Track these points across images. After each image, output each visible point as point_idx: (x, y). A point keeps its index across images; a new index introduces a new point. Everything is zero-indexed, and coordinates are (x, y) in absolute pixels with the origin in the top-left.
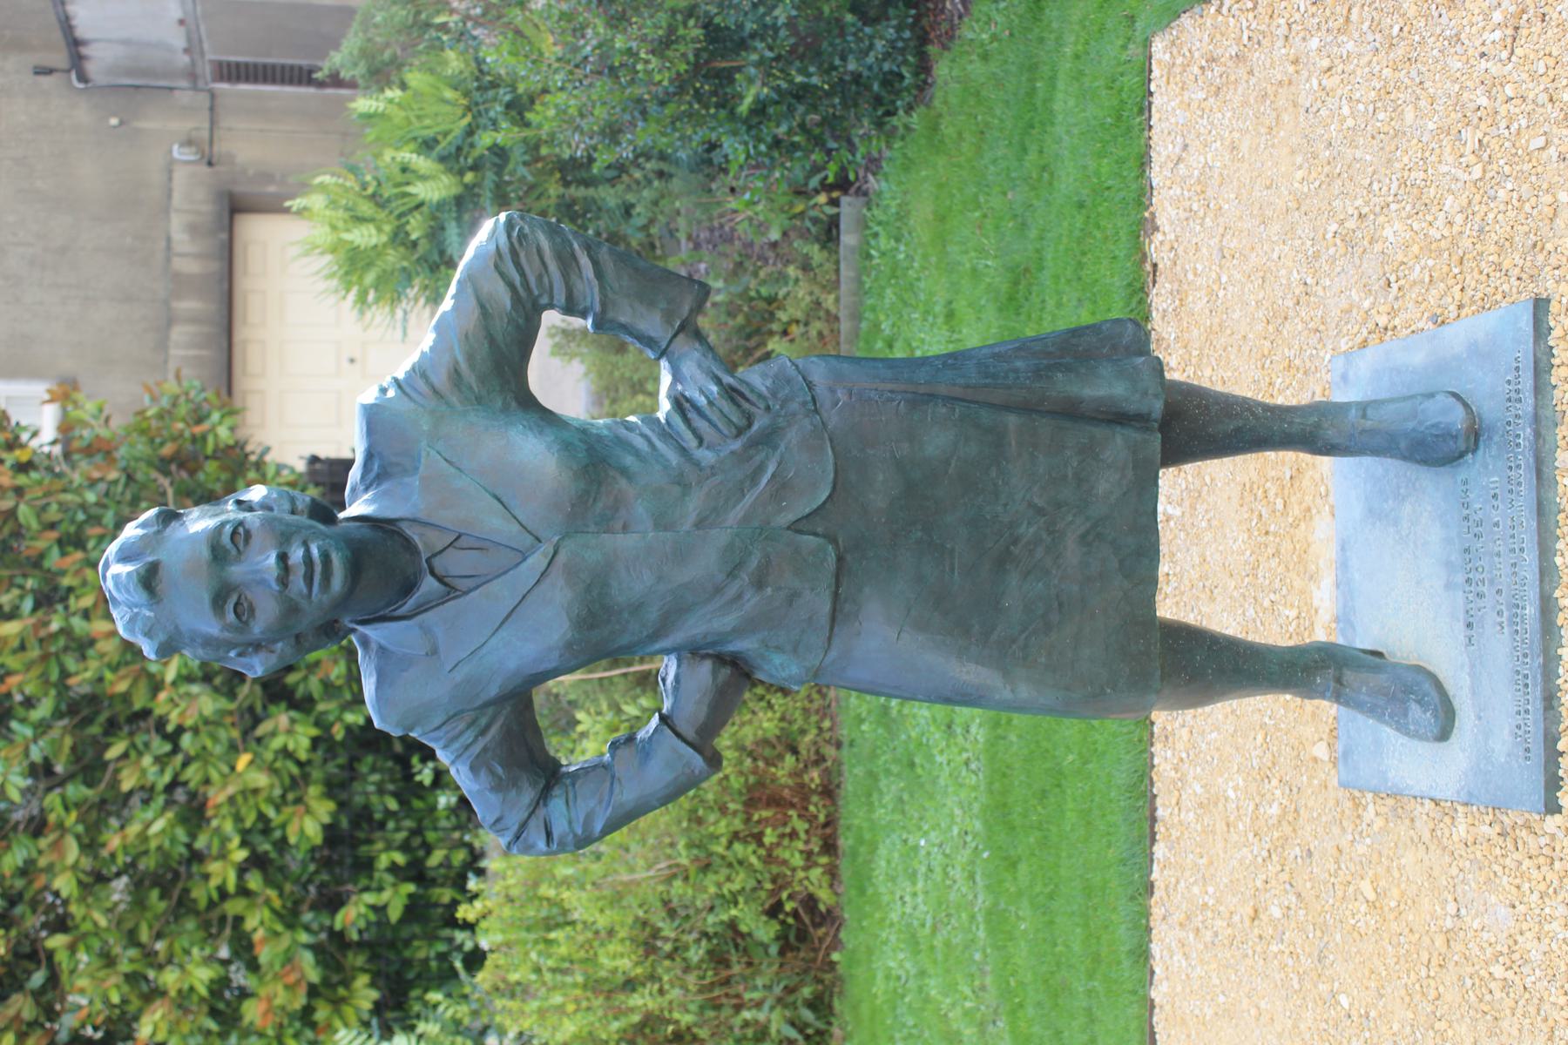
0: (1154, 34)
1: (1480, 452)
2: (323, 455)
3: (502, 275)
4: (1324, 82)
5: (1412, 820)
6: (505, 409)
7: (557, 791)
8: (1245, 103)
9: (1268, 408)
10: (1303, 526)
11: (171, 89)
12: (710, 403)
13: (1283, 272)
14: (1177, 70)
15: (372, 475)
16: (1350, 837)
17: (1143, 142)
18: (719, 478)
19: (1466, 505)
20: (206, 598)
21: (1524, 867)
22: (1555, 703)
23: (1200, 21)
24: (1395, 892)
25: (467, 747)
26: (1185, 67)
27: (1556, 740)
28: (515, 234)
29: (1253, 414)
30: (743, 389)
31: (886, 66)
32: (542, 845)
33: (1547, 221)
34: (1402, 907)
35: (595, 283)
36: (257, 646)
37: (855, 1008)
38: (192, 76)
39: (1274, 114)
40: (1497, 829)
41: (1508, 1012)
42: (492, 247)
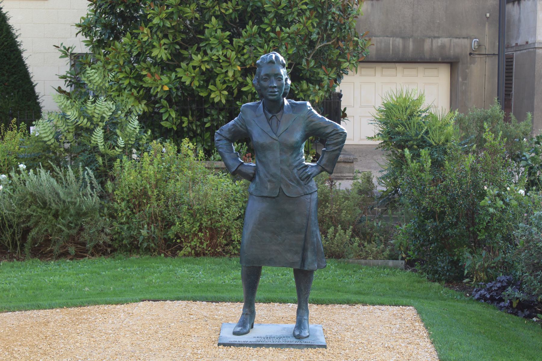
6: (305, 131)
7: (228, 142)
12: (306, 172)
18: (290, 172)
20: (268, 73)
27: (233, 346)
29: (306, 294)
30: (309, 179)
35: (332, 150)
36: (259, 82)
37: (147, 259)
42: (339, 129)
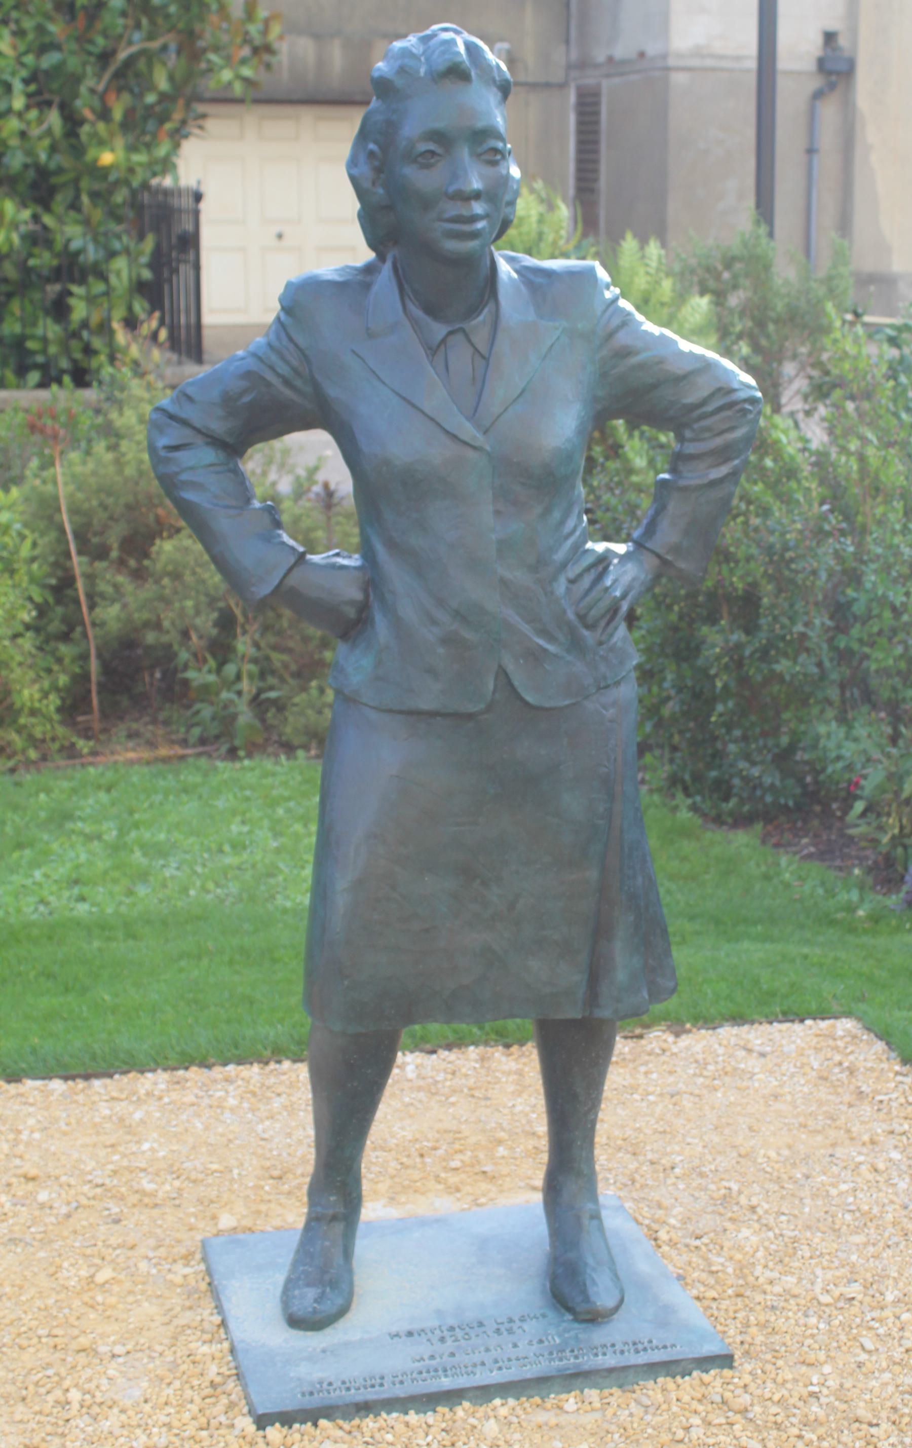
0: (859, 1019)
1: (576, 1325)
2: (203, 206)
3: (712, 395)
4: (863, 1167)
5: (190, 1308)
8: (820, 1103)
9: (594, 1123)
10: (441, 1187)
11: (567, 42)
13: (677, 1148)
14: (831, 1042)
15: (531, 276)
16: (151, 1255)
17: (756, 1017)
19: (522, 1319)
20: (439, 125)
21: (189, 1406)
22: (363, 1413)
23: (884, 1057)
24: (112, 1300)
25: (272, 368)
26: (836, 1048)
28: (748, 406)
31: (736, 781)
32: (162, 442)
33: (801, 1359)
34: (100, 1308)
35: (706, 481)
38: (583, 64)
39: (820, 1128)
40: (218, 1379)
41: (37, 1408)
42: (736, 386)
